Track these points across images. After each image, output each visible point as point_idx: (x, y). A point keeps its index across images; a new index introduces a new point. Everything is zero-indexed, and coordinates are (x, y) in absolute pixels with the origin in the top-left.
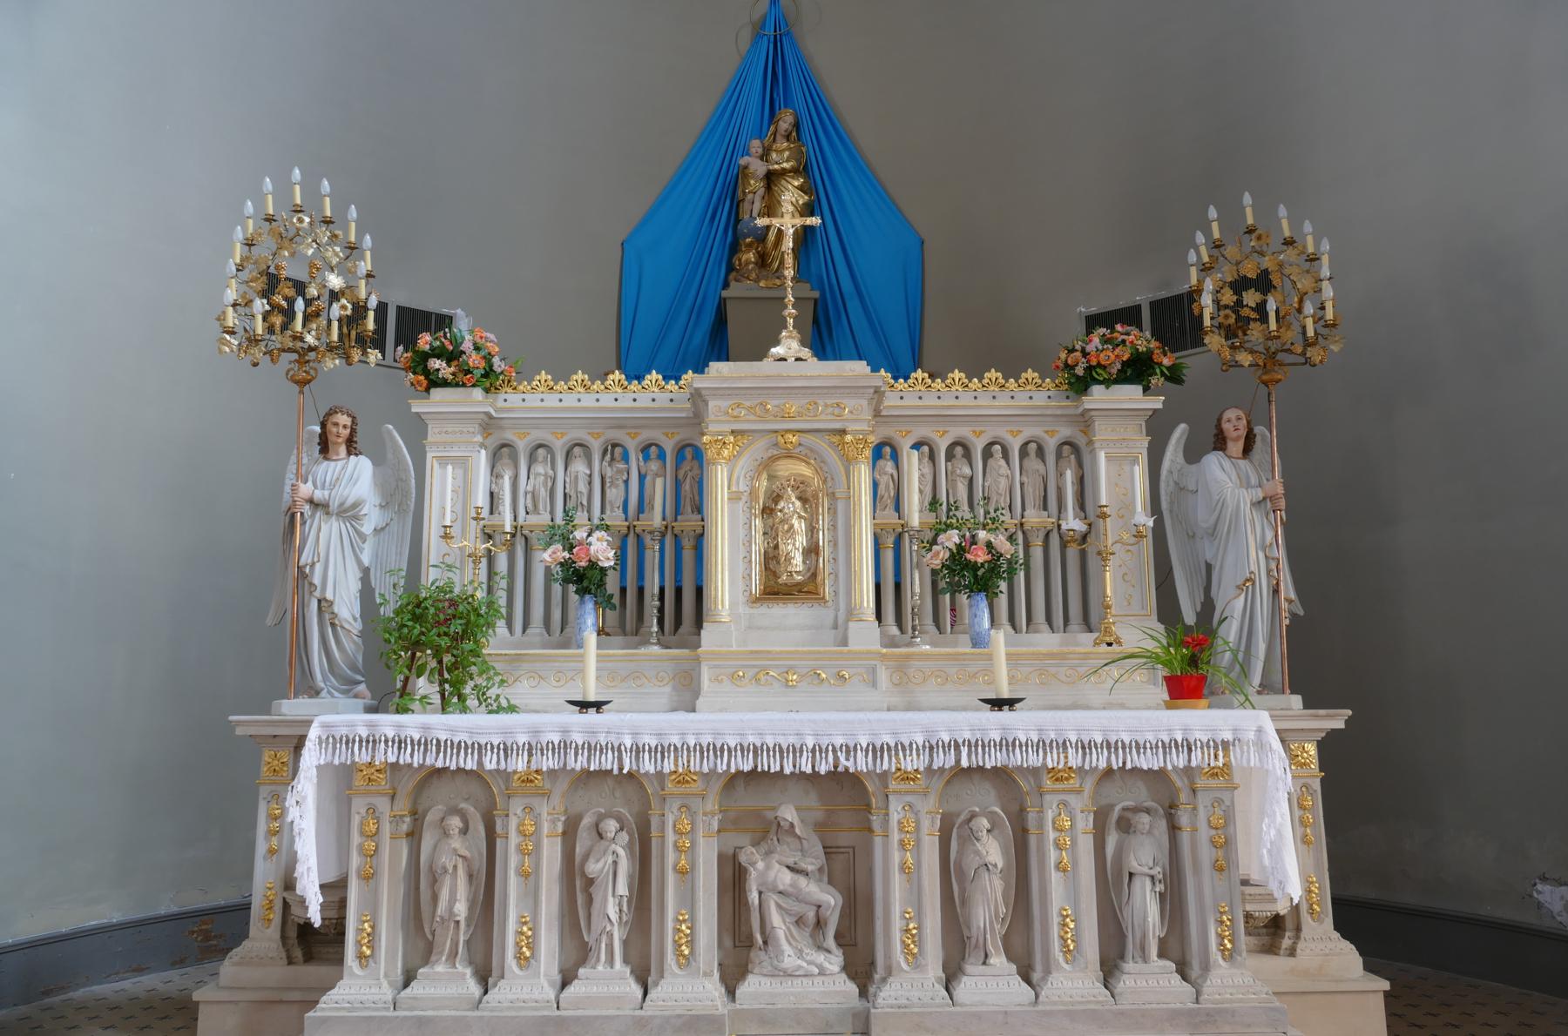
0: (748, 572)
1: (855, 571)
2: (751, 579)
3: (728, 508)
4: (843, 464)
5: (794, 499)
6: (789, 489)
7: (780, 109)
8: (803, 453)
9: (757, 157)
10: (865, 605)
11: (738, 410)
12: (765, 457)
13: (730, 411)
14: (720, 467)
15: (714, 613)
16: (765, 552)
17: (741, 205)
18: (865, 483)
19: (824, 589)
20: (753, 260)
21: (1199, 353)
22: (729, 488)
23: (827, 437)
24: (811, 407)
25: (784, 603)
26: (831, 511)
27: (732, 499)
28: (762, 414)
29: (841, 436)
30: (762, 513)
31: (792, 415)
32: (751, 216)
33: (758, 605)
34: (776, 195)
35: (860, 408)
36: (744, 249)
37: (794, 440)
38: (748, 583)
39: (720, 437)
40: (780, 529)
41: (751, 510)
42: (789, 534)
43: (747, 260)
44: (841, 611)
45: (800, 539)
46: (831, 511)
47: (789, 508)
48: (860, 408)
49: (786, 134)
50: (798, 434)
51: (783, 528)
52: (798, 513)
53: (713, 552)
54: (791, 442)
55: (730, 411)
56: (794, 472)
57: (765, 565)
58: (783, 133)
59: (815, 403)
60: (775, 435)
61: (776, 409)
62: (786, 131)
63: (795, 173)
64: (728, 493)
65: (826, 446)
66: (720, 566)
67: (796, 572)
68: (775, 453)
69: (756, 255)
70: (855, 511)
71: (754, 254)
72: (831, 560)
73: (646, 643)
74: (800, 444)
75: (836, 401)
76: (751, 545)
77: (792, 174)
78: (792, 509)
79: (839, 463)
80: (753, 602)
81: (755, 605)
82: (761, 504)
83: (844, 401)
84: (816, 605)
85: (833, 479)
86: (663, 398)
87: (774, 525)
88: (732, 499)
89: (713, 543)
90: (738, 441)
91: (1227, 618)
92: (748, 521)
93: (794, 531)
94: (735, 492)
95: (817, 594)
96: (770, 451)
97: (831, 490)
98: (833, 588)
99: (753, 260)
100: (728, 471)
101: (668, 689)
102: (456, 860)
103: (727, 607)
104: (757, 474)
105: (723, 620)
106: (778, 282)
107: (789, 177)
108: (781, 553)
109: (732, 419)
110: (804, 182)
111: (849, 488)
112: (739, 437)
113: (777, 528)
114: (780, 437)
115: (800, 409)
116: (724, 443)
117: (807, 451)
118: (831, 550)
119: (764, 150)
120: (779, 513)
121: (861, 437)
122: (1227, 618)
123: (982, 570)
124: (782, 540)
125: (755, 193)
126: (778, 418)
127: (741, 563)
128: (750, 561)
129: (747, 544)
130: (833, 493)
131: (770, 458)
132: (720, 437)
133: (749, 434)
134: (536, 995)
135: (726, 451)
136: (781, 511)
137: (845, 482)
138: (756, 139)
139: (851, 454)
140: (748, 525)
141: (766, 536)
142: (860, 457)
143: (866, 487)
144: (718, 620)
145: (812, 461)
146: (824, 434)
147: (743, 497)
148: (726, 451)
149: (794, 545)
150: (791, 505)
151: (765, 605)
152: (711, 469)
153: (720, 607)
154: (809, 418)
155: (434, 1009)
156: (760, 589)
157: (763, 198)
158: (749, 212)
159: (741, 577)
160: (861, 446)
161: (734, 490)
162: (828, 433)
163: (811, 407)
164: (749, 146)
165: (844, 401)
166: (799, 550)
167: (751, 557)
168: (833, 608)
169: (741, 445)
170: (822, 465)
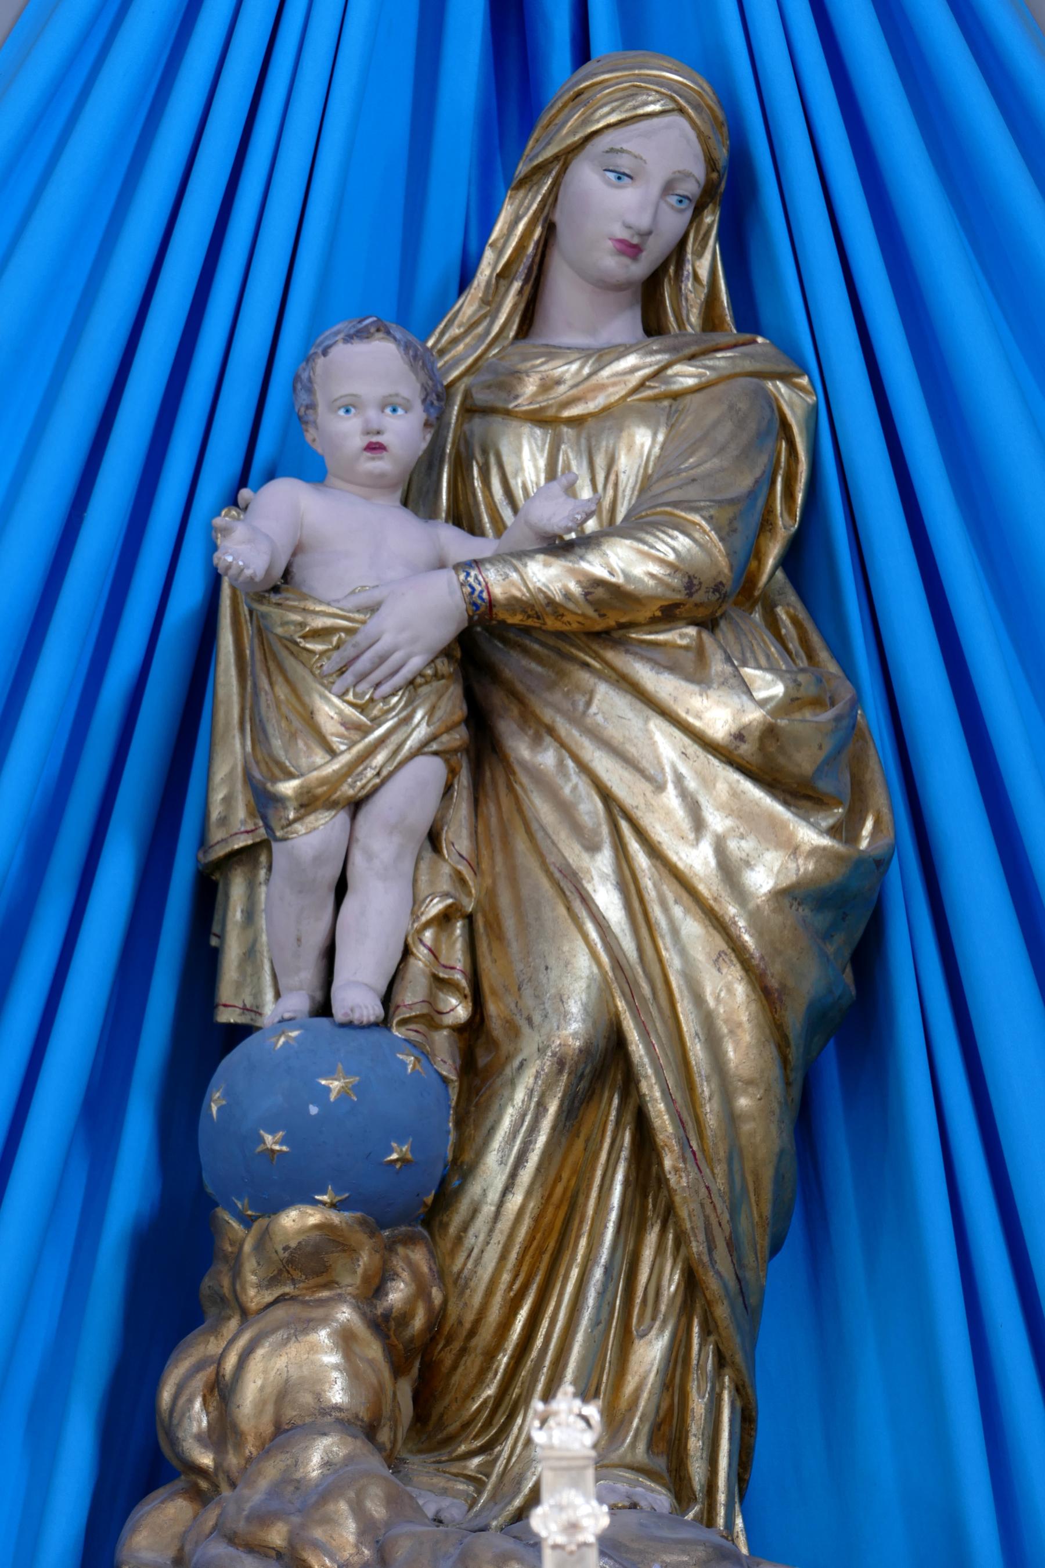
7: (582, 53)
9: (377, 484)
17: (237, 890)
20: (337, 1394)
32: (323, 1008)
34: (543, 810)
36: (254, 1296)
43: (284, 1394)
49: (640, 269)
58: (612, 264)
62: (631, 250)
63: (709, 624)
69: (374, 1350)
71: (346, 1340)
73: (372, 1234)
77: (684, 635)
91: (775, 1248)
96: (450, 1090)
99: (337, 1394)
101: (512, 652)
102: (404, 1022)
107: (652, 654)
110: (791, 704)
119: (435, 424)
122: (775, 1248)
125: (356, 806)
134: (407, 999)
138: (361, 334)
157: (433, 838)
158: (308, 974)
164: (301, 384)
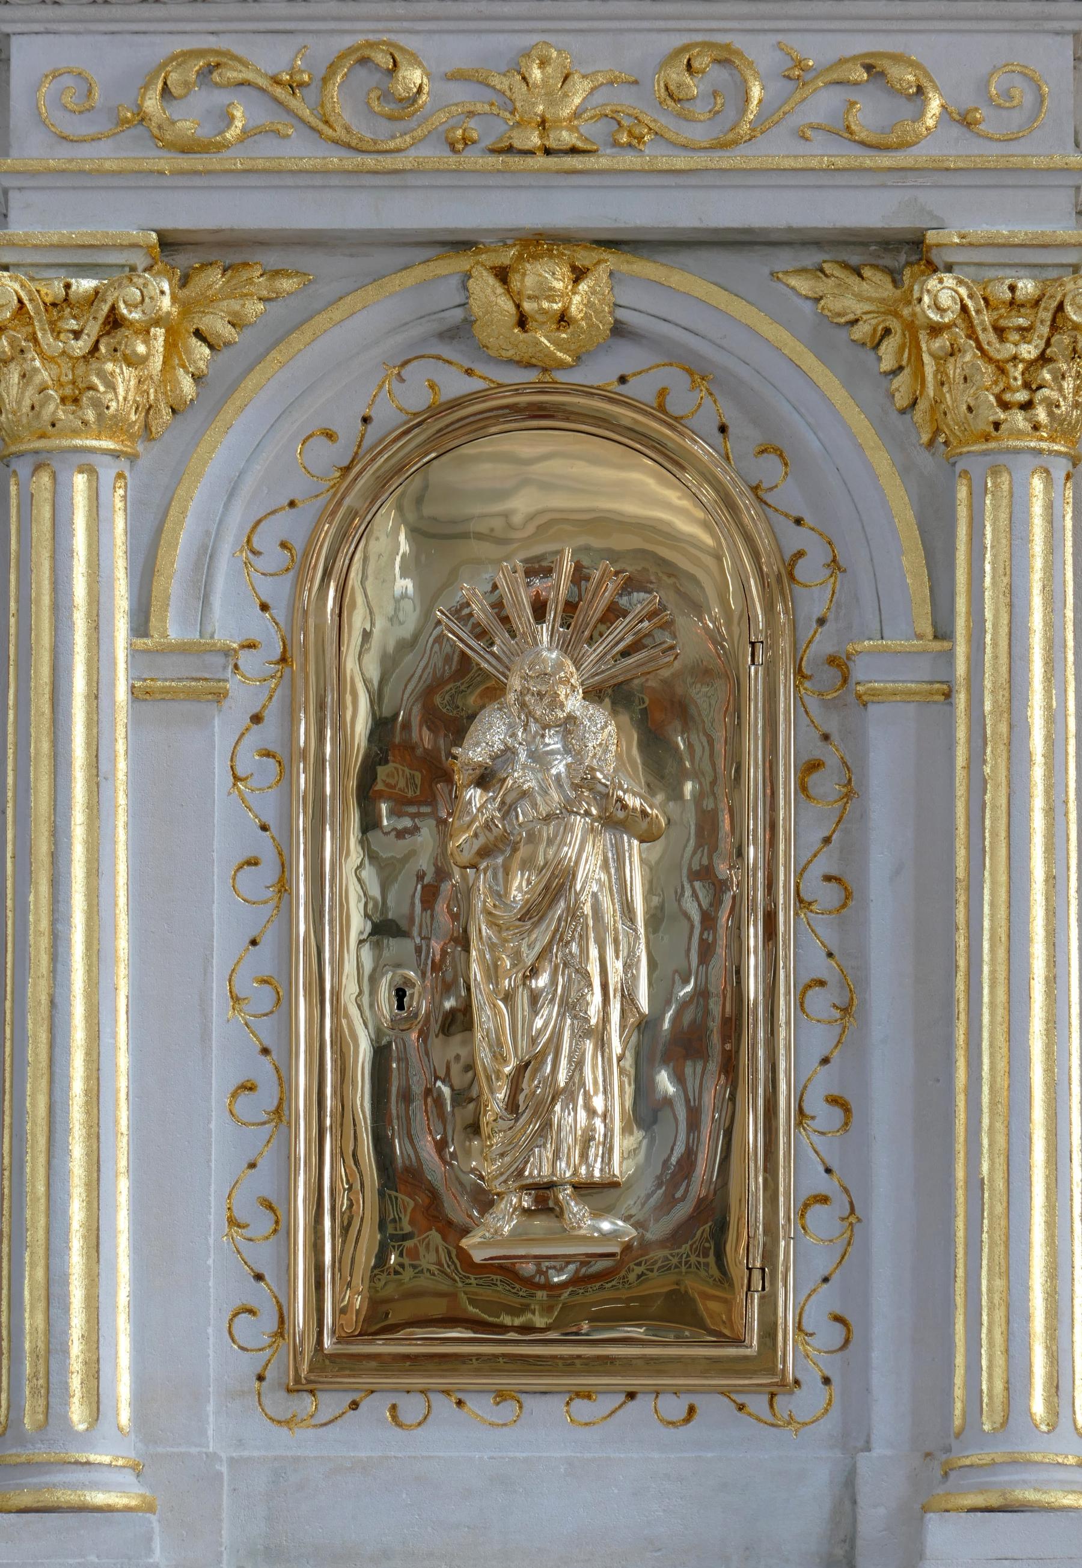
0: (263, 1182)
1: (975, 1184)
2: (282, 1228)
3: (135, 755)
4: (905, 470)
5: (574, 703)
6: (544, 633)
8: (642, 389)
10: (1038, 1406)
11: (202, 100)
12: (386, 416)
13: (152, 103)
14: (80, 481)
15: (40, 1453)
16: (381, 1054)
18: (1052, 602)
19: (769, 1302)
21: (690, 938)
22: (140, 626)
23: (803, 285)
24: (693, 86)
25: (501, 1396)
26: (827, 784)
27: (168, 695)
28: (363, 129)
29: (895, 277)
30: (367, 796)
31: (568, 138)
33: (331, 1403)
35: (1022, 94)
37: (576, 306)
38: (263, 1257)
39: (85, 285)
40: (482, 899)
41: (286, 774)
42: (541, 936)
44: (879, 1450)
45: (615, 967)
46: (827, 784)
47: (540, 759)
48: (1022, 94)
50: (612, 260)
51: (501, 896)
52: (603, 797)
53: (37, 1051)
54: (563, 319)
55: (152, 103)
56: (559, 501)
57: (381, 1143)
59: (726, 59)
60: (463, 263)
61: (460, 94)
64: (134, 653)
65: (792, 346)
66: (77, 1150)
67: (584, 1189)
68: (455, 385)
70: (978, 785)
72: (815, 1105)
74: (619, 330)
75: (862, 45)
76: (283, 1003)
78: (559, 767)
79: (882, 462)
80: (298, 1387)
81: (307, 1403)
82: (361, 726)
83: (916, 47)
84: (712, 1407)
85: (835, 565)
86: (59, 1494)
87: (442, 874)
88: (168, 695)
89: (38, 991)
90: (208, 302)
92: (265, 847)
93: (573, 913)
94: (183, 649)
95: (738, 1342)
96: (418, 373)
97: (823, 644)
98: (825, 1301)
100: (135, 511)
103: (125, 1416)
104: (329, 530)
105: (99, 1498)
106: (138, 684)
108: (484, 1056)
109: (165, 162)
111: (943, 633)
112: (215, 278)
113: (467, 893)
114: (486, 286)
115: (626, 99)
116: (114, 322)
117: (675, 379)
118: (820, 1040)
120: (475, 796)
121: (1027, 287)
123: (500, 1238)
124: (493, 972)
126: (474, 159)
127: (218, 1122)
128: (281, 1112)
129: (264, 999)
130: (839, 664)
131: (418, 421)
132: (85, 285)
133: (273, 259)
135: (125, 379)
136: (485, 779)
137: (917, 583)
139: (956, 400)
140: (268, 871)
141: (394, 946)
142: (1019, 419)
143: (1052, 626)
144: (49, 1498)
145: (701, 450)
146: (785, 259)
147: (233, 684)
148: (125, 379)
149: (572, 1006)
150: (553, 742)
151: (376, 1406)
152: (28, 501)
153: (77, 1414)
154: (681, 162)
155: (9, 1254)
156: (341, 1311)
159: (215, 1216)
160: (1029, 351)
161: (174, 632)
162: (811, 258)
163: (693, 86)
165: (916, 47)
166: (602, 1044)
167: (284, 1081)
168: (828, 1426)
169: (227, 332)
170: (769, 469)
